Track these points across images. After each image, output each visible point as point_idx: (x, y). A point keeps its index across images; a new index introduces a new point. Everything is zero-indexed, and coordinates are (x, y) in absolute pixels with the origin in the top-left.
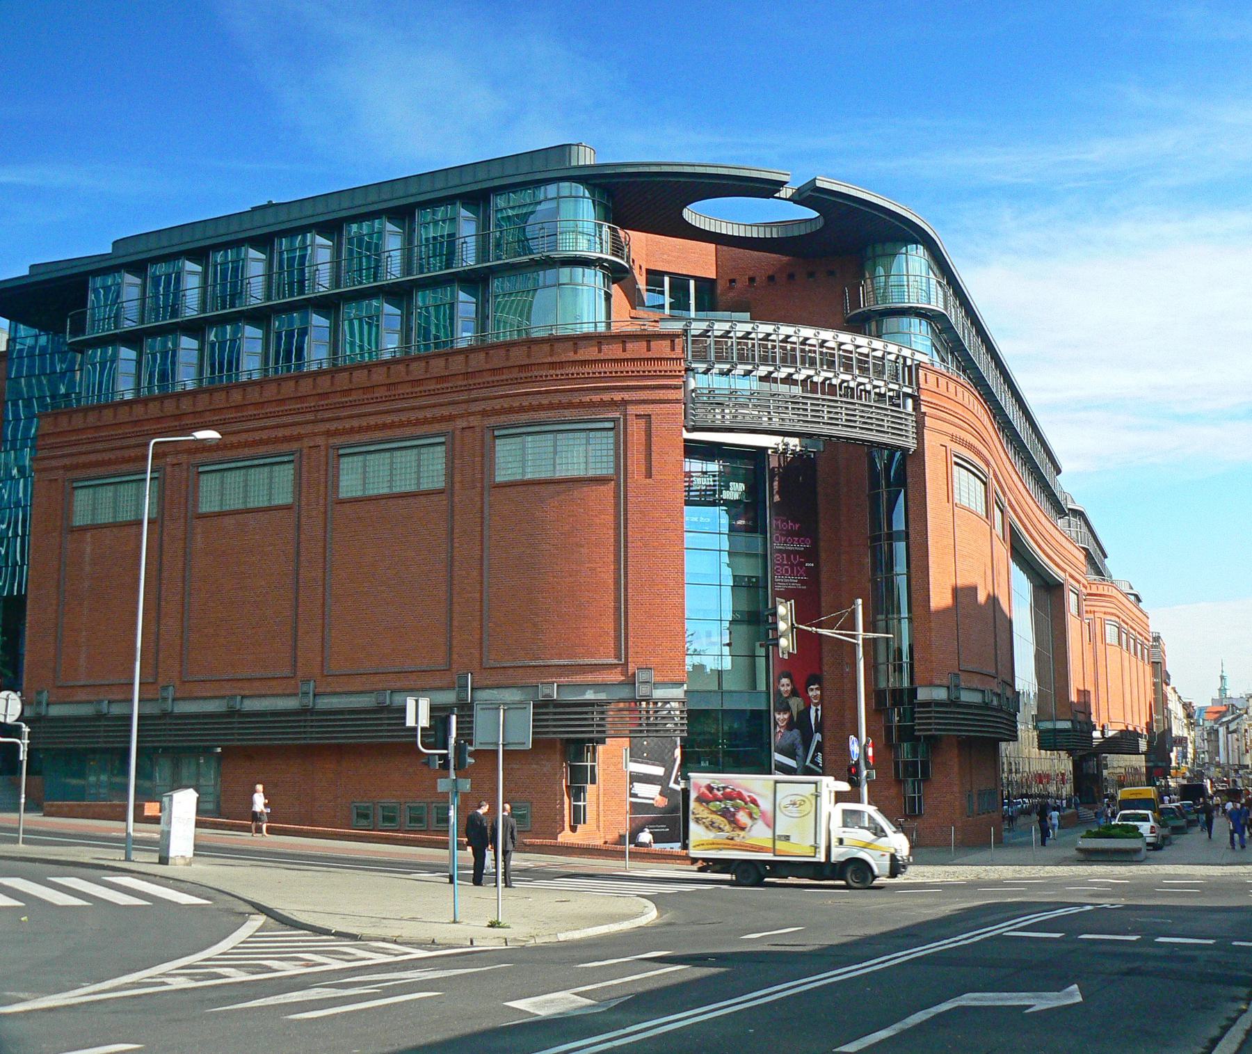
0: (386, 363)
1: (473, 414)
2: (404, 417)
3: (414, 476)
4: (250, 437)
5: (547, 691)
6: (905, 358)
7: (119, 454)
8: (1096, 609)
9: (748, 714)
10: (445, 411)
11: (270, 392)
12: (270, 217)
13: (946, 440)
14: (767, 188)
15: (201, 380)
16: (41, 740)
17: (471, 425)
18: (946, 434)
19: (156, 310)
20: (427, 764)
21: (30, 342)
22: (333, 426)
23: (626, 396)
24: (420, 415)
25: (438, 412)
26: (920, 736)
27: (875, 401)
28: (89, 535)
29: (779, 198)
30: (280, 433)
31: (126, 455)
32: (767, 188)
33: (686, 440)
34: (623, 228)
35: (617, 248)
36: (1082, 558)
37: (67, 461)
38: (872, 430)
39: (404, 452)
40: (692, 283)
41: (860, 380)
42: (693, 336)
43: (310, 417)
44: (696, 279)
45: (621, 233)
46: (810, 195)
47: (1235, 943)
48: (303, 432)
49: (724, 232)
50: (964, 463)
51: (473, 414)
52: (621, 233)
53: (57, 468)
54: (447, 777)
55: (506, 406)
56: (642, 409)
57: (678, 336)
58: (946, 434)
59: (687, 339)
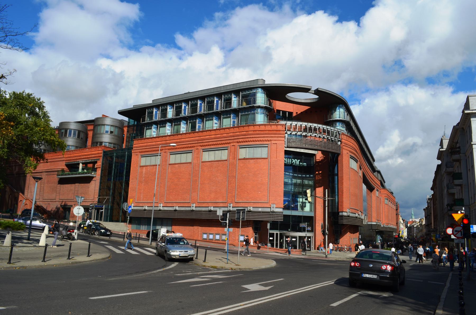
0: (215, 130)
1: (166, 149)
2: (254, 139)
3: (260, 153)
4: (213, 143)
5: (250, 208)
6: (339, 132)
7: (152, 149)
8: (383, 195)
9: (297, 216)
10: (228, 141)
11: (262, 128)
12: (188, 95)
13: (348, 152)
14: (306, 90)
15: (171, 133)
16: (145, 214)
17: (234, 145)
18: (348, 150)
19: (206, 111)
20: (221, 224)
21: (133, 123)
22: (201, 144)
23: (271, 139)
24: (223, 142)
25: (227, 142)
26: (339, 224)
27: (331, 142)
28: (144, 168)
29: (309, 93)
30: (189, 145)
31: (249, 140)
32: (306, 90)
33: (285, 150)
34: (272, 100)
35: (270, 104)
36: (380, 182)
37: (140, 151)
38: (326, 148)
39: (264, 148)
40: (287, 113)
41: (328, 136)
42: (287, 125)
43: (196, 142)
44: (282, 111)
45: (271, 100)
46: (317, 92)
47: (429, 282)
48: (195, 145)
49: (295, 101)
50: (352, 158)
51: (166, 149)
52: (271, 100)
53: (138, 152)
54: (226, 227)
55: (242, 141)
56: (276, 142)
57: (284, 125)
58: (348, 150)
59: (286, 126)
